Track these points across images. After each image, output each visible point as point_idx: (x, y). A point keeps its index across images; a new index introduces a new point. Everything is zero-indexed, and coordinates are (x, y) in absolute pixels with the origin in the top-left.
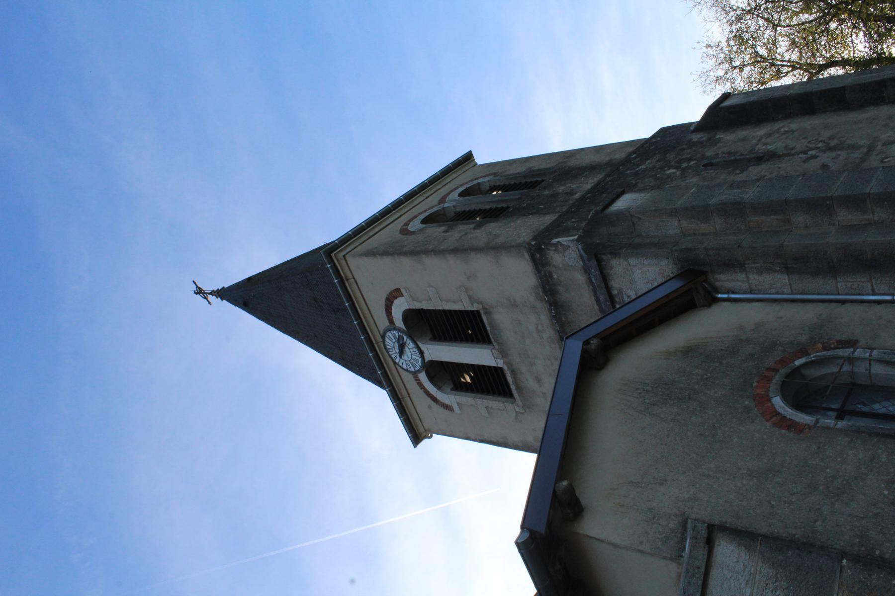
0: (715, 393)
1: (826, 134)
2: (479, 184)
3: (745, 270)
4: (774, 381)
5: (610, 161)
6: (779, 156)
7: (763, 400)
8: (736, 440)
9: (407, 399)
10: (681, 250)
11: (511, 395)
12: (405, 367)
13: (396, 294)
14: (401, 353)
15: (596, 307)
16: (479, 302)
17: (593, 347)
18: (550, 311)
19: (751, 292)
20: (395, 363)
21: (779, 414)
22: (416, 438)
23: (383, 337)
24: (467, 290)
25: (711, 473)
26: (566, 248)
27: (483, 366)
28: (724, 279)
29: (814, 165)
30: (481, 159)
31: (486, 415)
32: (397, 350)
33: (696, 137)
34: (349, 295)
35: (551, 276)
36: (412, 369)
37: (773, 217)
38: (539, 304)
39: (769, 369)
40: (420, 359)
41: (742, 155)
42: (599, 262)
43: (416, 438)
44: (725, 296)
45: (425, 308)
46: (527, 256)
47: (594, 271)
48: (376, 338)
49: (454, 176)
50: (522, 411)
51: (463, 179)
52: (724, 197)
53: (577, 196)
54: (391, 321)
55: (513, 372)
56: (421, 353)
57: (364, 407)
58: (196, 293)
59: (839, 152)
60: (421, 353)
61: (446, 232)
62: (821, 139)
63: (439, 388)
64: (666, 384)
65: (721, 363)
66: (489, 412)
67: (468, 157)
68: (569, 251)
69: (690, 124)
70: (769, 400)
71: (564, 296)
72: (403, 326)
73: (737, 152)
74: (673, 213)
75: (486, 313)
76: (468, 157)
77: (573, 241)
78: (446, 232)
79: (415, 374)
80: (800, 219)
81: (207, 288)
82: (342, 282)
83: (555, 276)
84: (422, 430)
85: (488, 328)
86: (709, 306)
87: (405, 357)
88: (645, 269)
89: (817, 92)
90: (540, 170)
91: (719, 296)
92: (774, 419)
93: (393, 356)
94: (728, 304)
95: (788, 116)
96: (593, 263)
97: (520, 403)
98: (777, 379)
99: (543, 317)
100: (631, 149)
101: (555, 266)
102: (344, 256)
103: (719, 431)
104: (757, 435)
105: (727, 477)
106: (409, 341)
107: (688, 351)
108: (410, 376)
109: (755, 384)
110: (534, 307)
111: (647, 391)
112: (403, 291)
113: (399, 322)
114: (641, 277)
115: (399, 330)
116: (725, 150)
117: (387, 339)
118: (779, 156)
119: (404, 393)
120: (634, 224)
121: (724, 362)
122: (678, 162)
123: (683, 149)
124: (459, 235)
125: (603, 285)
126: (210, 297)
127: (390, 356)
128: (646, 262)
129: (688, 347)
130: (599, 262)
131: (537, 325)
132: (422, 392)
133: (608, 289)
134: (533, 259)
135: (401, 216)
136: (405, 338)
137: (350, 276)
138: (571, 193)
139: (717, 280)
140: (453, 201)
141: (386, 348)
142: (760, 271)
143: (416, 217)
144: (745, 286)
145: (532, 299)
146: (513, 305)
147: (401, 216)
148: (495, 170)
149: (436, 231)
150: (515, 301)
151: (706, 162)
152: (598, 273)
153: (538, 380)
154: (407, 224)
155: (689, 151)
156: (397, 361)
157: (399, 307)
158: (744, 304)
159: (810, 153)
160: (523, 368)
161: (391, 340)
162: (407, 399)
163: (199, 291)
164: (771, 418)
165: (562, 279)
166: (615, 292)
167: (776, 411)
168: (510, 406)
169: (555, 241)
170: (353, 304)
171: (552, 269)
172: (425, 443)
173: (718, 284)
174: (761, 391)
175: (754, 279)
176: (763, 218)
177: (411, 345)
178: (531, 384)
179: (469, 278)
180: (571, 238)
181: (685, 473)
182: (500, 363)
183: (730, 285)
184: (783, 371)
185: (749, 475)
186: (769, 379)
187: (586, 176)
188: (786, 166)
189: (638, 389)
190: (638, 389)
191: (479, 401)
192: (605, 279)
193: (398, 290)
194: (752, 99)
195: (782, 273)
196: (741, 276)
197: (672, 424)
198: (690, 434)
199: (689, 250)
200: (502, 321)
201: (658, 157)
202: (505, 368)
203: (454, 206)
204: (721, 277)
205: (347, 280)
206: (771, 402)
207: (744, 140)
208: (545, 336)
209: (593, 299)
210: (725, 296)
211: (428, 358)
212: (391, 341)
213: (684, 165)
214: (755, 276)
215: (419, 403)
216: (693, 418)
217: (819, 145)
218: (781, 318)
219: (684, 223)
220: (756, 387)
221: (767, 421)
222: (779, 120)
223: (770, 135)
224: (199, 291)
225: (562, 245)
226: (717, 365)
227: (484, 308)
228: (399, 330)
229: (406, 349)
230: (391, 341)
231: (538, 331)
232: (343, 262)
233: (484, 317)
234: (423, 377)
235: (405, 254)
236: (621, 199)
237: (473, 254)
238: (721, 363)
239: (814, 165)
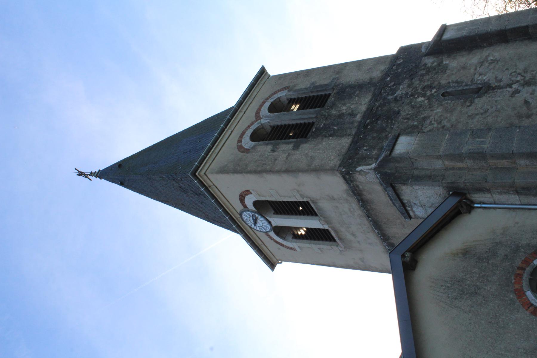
0: (491, 288)
1: (521, 66)
2: (279, 98)
3: (490, 192)
4: (524, 278)
5: (371, 79)
6: (494, 89)
7: (520, 294)
8: (511, 326)
9: (263, 246)
10: (448, 183)
11: (334, 241)
12: (258, 229)
13: (248, 192)
14: (255, 223)
15: (390, 202)
16: (307, 197)
17: (408, 259)
18: (359, 204)
19: (495, 204)
20: (251, 228)
21: (532, 305)
22: (272, 265)
23: (241, 214)
24: (298, 191)
25: (503, 352)
26: (366, 173)
27: (315, 229)
28: (476, 197)
29: (519, 99)
30: (272, 71)
31: (320, 252)
32: (253, 222)
33: (429, 61)
34: (213, 195)
35: (358, 186)
36: (264, 231)
37: (504, 161)
38: (349, 198)
39: (519, 268)
40: (269, 226)
41: (467, 85)
42: (394, 188)
43: (272, 265)
44: (479, 205)
45: (269, 200)
46: (339, 175)
47: (391, 193)
48: (236, 216)
49: (258, 89)
50: (344, 250)
51: (263, 92)
52: (470, 147)
53: (358, 118)
54: (245, 206)
55: (336, 231)
56: (270, 223)
57: (228, 245)
58: (79, 175)
59: (534, 88)
60: (270, 223)
61: (273, 151)
62: (518, 71)
63: (284, 239)
64: (459, 282)
65: (488, 263)
66: (321, 251)
67: (263, 71)
68: (369, 174)
69: (420, 46)
70: (524, 294)
71: (367, 196)
72: (254, 209)
73: (462, 82)
74: (439, 157)
75: (313, 203)
76: (263, 71)
77: (371, 169)
78: (273, 151)
79: (266, 233)
80: (522, 162)
81: (87, 171)
82: (207, 189)
83: (361, 187)
84: (275, 260)
85: (316, 210)
86: (469, 212)
87: (258, 225)
88: (425, 191)
89: (509, 30)
90: (321, 86)
91: (476, 205)
92: (530, 308)
93: (249, 224)
94: (481, 210)
95: (490, 45)
96: (390, 189)
97: (342, 246)
98: (526, 276)
99: (353, 205)
100: (383, 67)
101: (360, 182)
102: (205, 174)
103: (500, 320)
104: (523, 322)
105: (513, 355)
106: (259, 217)
107: (466, 253)
108: (264, 234)
109: (513, 281)
110: (347, 200)
111: (448, 287)
112: (252, 191)
113: (250, 206)
114: (425, 199)
115: (252, 211)
116: (454, 78)
117: (243, 216)
118: (494, 89)
119: (260, 243)
120: (412, 163)
121: (490, 262)
122: (423, 89)
123: (423, 75)
124: (285, 156)
125: (398, 199)
126: (90, 177)
127: (247, 224)
128: (425, 188)
129: (464, 249)
130: (394, 188)
131: (350, 209)
132: (272, 241)
133: (401, 201)
134: (344, 177)
135: (232, 132)
136: (257, 215)
137: (211, 184)
138: (353, 115)
139: (472, 197)
140: (268, 119)
141: (243, 221)
142: (500, 193)
143: (244, 133)
144: (491, 200)
145: (345, 196)
146: (332, 199)
147: (232, 132)
148: (286, 84)
149: (265, 149)
150: (333, 197)
151: (443, 91)
152: (393, 193)
153: (353, 235)
154: (240, 141)
155: (427, 77)
156: (253, 226)
157: (249, 201)
158: (492, 210)
159: (514, 86)
160: (343, 229)
161: (247, 216)
162: (263, 246)
163: (81, 174)
164: (528, 308)
165: (366, 188)
166: (405, 201)
167: (530, 303)
168: (335, 248)
169: (359, 169)
170: (216, 199)
171: (358, 183)
172: (278, 266)
173: (473, 199)
174: (517, 287)
175: (497, 197)
176: (499, 161)
177: (262, 219)
178: (349, 237)
179: (299, 185)
180: (370, 167)
181: (487, 353)
182: (326, 227)
183: (482, 199)
184: (528, 270)
185: (525, 353)
186: (520, 276)
187: (357, 96)
188: (501, 98)
189: (442, 286)
190: (442, 286)
191: (314, 246)
192: (398, 196)
193: (248, 191)
194: (464, 33)
195: (514, 194)
196: (489, 195)
197: (470, 315)
198: (483, 322)
199: (453, 183)
200: (325, 206)
201: (406, 82)
202: (330, 229)
203: (269, 122)
204: (475, 195)
205: (210, 187)
206: (525, 295)
207: (464, 68)
208: (356, 214)
209: (388, 198)
210: (479, 205)
211: (274, 224)
212: (246, 216)
213: (428, 93)
214: (498, 196)
215: (271, 246)
216: (482, 310)
217: (518, 79)
218: (517, 223)
219: (447, 163)
220: (515, 283)
221: (527, 310)
222: (484, 47)
223: (481, 64)
224: (81, 174)
225: (363, 171)
226: (486, 264)
227: (311, 200)
228: (252, 211)
229: (258, 221)
230: (246, 216)
231: (351, 212)
232: (205, 177)
233: (312, 205)
234: (272, 234)
235: (250, 172)
236: (399, 142)
237: (300, 174)
238: (488, 263)
239: (519, 99)
